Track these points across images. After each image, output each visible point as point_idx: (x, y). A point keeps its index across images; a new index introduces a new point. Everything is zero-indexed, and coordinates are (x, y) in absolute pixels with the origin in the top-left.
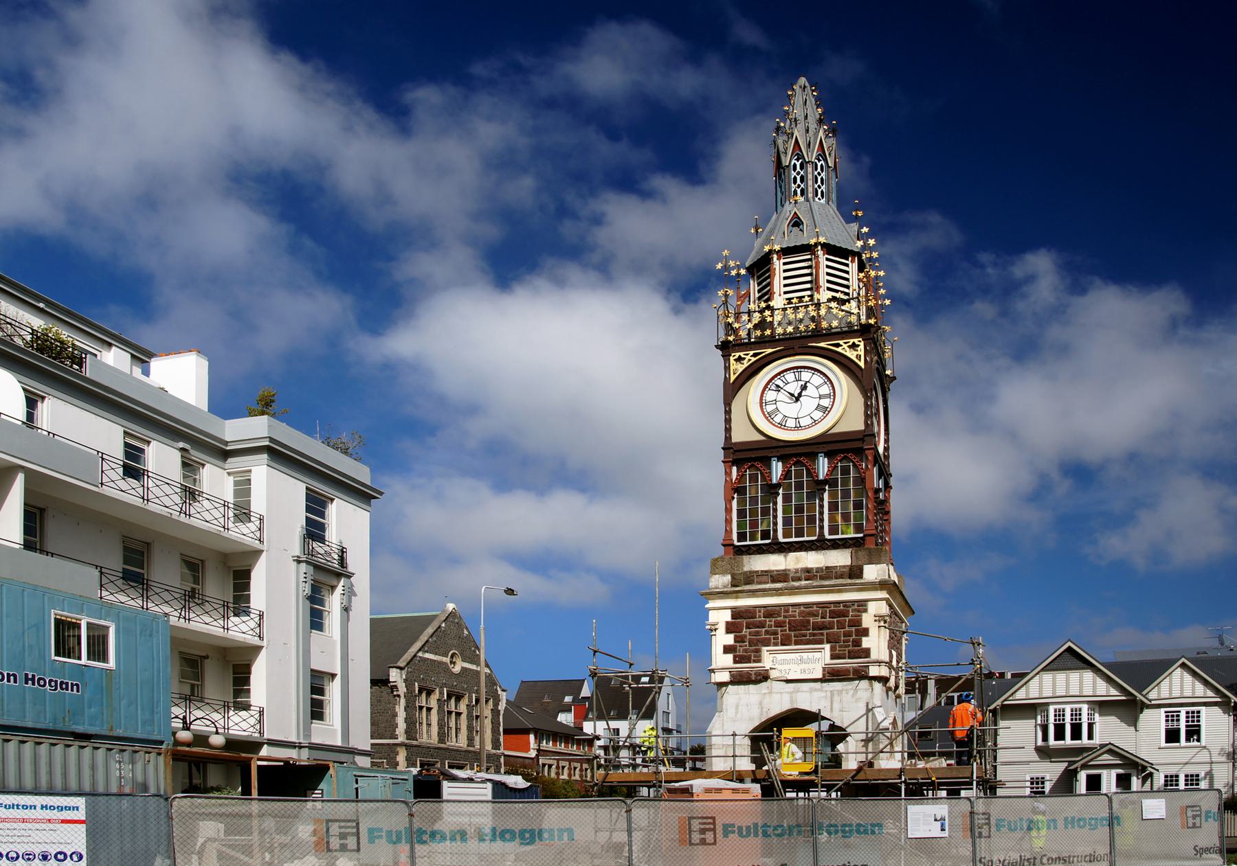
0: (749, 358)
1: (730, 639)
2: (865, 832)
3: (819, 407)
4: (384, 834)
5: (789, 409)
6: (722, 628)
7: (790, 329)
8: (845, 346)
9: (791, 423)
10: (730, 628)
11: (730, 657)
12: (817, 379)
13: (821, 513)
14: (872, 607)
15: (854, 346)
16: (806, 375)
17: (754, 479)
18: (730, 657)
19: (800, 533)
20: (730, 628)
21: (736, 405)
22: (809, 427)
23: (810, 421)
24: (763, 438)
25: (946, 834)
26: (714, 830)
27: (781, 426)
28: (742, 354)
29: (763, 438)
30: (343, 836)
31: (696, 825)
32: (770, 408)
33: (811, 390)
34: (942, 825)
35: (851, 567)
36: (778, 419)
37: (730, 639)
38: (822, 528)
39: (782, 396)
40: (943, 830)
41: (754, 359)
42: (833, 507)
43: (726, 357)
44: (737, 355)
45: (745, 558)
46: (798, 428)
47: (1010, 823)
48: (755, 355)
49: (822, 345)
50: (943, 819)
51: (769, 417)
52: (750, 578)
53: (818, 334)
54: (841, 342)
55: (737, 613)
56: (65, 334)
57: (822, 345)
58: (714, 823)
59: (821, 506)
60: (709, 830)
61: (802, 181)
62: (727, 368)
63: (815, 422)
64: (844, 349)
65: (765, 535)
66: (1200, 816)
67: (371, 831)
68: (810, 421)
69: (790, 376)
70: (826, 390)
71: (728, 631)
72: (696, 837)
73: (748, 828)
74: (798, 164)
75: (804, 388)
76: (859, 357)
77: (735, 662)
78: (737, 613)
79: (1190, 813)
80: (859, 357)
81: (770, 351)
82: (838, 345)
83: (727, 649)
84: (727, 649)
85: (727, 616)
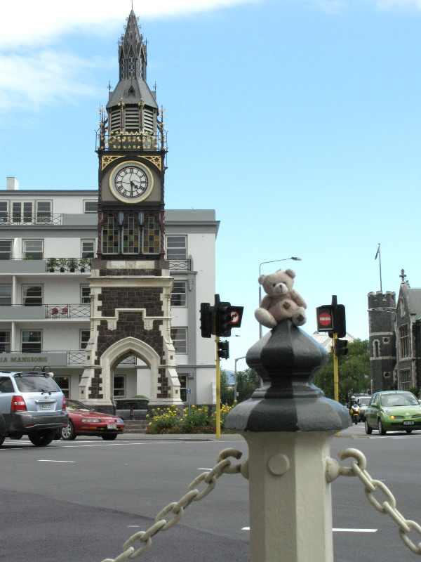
0: (111, 159)
1: (100, 303)
6: (97, 297)
7: (129, 147)
9: (143, 179)
10: (100, 298)
11: (100, 312)
13: (121, 241)
14: (165, 291)
17: (131, 220)
18: (100, 312)
19: (111, 250)
20: (100, 298)
21: (104, 180)
27: (124, 195)
32: (119, 185)
35: (155, 270)
36: (122, 191)
37: (100, 303)
38: (121, 249)
42: (126, 238)
43: (100, 157)
45: (108, 262)
51: (119, 189)
52: (110, 272)
53: (142, 152)
55: (104, 289)
56: (200, 476)
59: (121, 238)
62: (100, 164)
64: (152, 160)
65: (136, 250)
69: (122, 174)
70: (143, 179)
71: (99, 300)
74: (132, 59)
77: (103, 315)
78: (104, 289)
80: (159, 165)
82: (150, 158)
83: (99, 309)
84: (99, 309)
85: (99, 291)
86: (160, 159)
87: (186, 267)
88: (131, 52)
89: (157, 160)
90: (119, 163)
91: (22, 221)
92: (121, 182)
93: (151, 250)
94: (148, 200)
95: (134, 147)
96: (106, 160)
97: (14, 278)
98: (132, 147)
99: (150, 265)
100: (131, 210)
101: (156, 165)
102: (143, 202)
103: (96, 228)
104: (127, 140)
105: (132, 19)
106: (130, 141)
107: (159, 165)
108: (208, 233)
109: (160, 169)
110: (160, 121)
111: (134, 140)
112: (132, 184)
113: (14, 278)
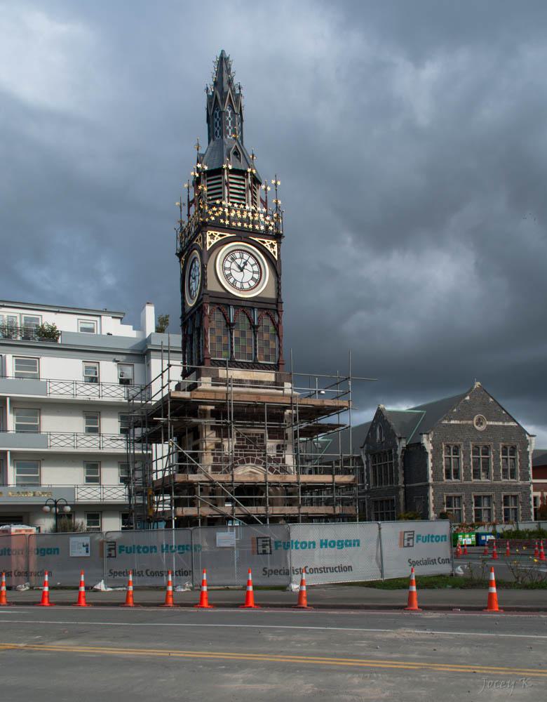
2: (350, 544)
3: (253, 278)
4: (125, 549)
5: (237, 275)
8: (268, 244)
9: (238, 285)
12: (252, 261)
15: (212, 236)
16: (246, 256)
22: (237, 289)
23: (248, 287)
24: (224, 291)
25: (89, 555)
26: (115, 549)
27: (233, 285)
28: (213, 232)
29: (224, 291)
30: (110, 550)
31: (106, 547)
32: (227, 272)
33: (248, 267)
34: (87, 549)
36: (232, 280)
39: (234, 266)
40: (87, 552)
41: (220, 238)
44: (211, 232)
46: (242, 289)
47: (284, 543)
48: (264, 242)
49: (257, 239)
50: (87, 545)
53: (255, 233)
54: (266, 241)
57: (257, 239)
58: (115, 545)
60: (411, 538)
61: (220, 125)
63: (251, 288)
64: (267, 243)
65: (249, 356)
66: (413, 538)
67: (418, 536)
68: (248, 287)
70: (256, 268)
72: (406, 542)
73: (131, 548)
75: (245, 264)
76: (210, 243)
79: (406, 537)
81: (228, 235)
86: (276, 245)
87: (123, 394)
88: (222, 104)
89: (272, 246)
90: (228, 243)
91: (176, 497)
92: (230, 269)
93: (267, 358)
94: (260, 296)
95: (245, 225)
96: (212, 236)
97: (9, 453)
98: (242, 225)
99: (269, 376)
100: (245, 306)
101: (272, 252)
102: (256, 297)
103: (181, 350)
104: (236, 215)
105: (223, 62)
106: (239, 216)
107: (274, 252)
108: (59, 415)
109: (276, 257)
110: (265, 200)
111: (245, 216)
112: (242, 270)
113: (9, 453)
